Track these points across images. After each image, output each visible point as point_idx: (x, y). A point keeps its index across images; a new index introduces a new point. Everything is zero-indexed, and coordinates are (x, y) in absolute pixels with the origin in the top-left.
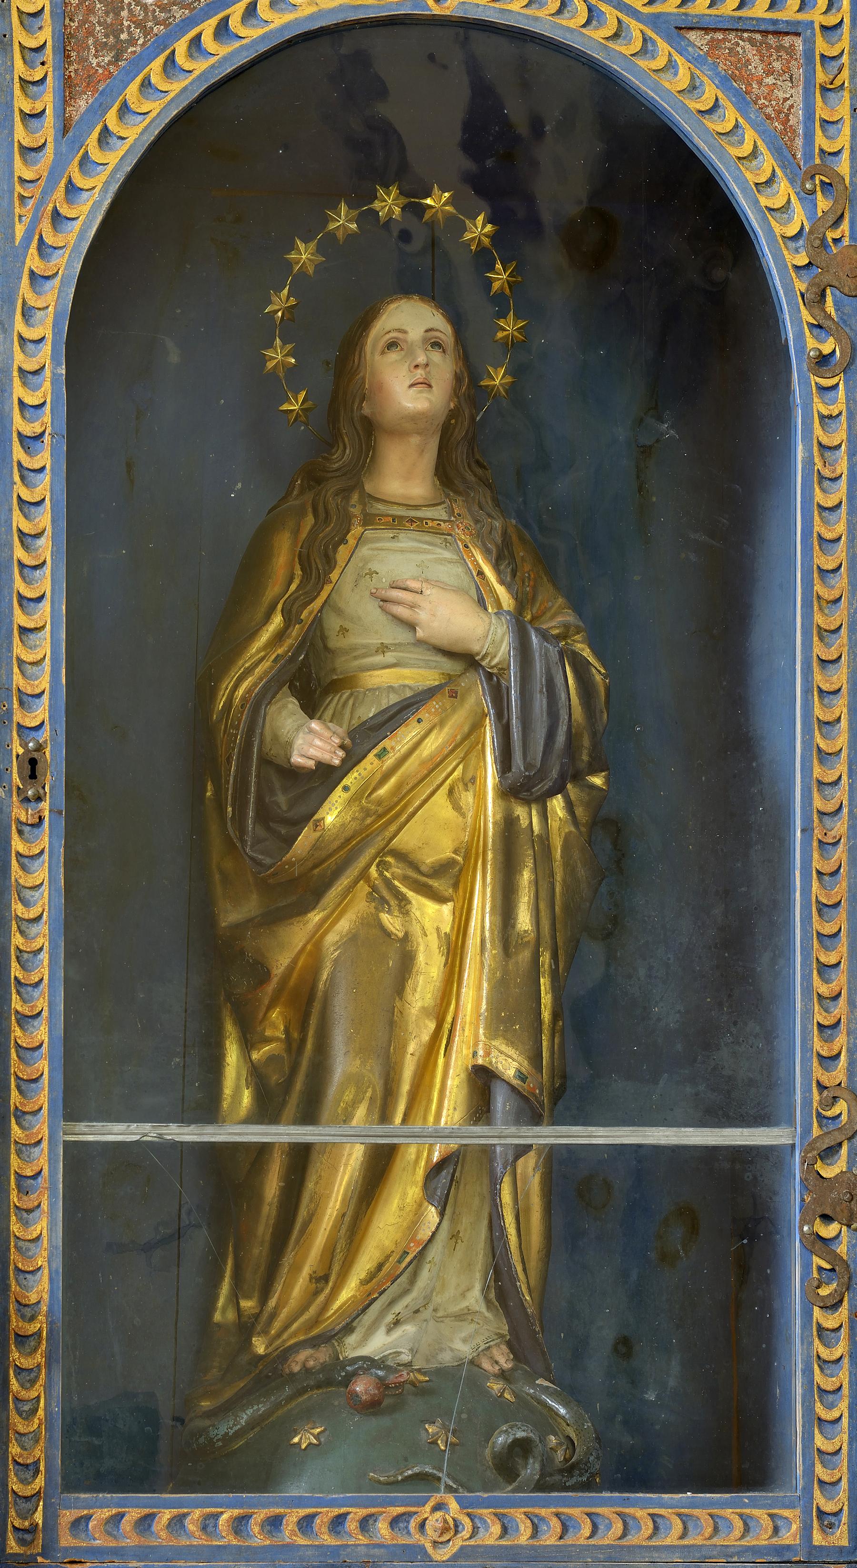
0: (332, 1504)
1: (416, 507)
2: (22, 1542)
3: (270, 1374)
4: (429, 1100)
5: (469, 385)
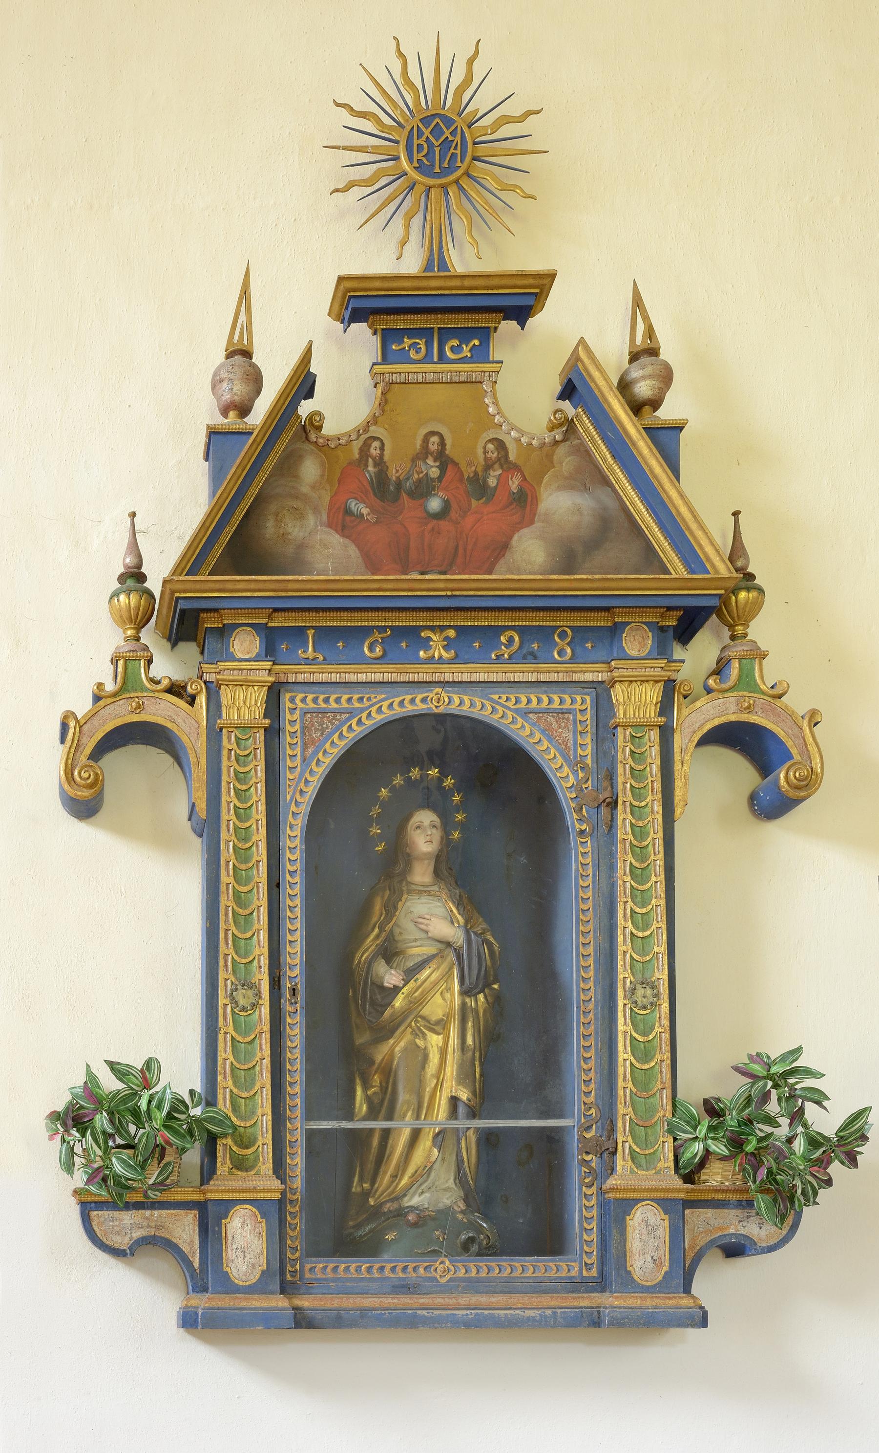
0: (403, 1262)
1: (427, 886)
2: (292, 1276)
3: (376, 1213)
4: (434, 1109)
5: (446, 841)
